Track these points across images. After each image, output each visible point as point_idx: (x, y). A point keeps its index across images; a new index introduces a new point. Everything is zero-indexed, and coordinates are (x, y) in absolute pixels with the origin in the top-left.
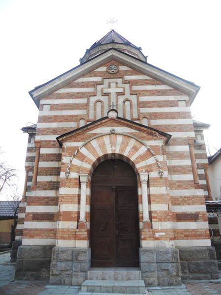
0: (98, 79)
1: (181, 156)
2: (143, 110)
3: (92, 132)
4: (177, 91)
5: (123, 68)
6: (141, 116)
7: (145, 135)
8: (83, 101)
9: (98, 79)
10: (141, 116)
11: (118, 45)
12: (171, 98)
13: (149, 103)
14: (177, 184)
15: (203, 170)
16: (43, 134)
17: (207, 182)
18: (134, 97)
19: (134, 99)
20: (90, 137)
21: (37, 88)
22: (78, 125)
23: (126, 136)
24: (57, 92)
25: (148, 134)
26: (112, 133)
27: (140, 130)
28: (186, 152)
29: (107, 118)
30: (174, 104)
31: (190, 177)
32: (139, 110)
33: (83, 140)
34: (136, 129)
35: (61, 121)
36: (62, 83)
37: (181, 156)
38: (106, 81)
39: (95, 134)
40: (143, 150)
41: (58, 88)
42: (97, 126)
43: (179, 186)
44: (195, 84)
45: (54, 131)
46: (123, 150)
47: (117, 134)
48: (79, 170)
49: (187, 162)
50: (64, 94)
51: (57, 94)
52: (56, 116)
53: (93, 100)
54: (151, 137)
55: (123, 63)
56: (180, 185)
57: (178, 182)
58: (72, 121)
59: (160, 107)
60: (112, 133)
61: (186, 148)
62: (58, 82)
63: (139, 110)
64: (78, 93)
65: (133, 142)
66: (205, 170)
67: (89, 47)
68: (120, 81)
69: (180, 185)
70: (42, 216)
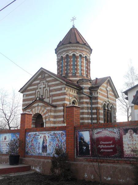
1: (60, 111)
3: (33, 106)
7: (46, 105)
8: (34, 92)
9: (38, 82)
11: (66, 45)
12: (60, 87)
14: (58, 122)
15: (96, 110)
17: (97, 116)
18: (49, 88)
19: (48, 89)
21: (21, 89)
24: (28, 89)
25: (47, 105)
26: (38, 106)
28: (61, 110)
29: (36, 100)
30: (61, 89)
31: (62, 119)
33: (31, 109)
34: (44, 103)
35: (29, 101)
36: (28, 85)
37: (60, 111)
39: (34, 106)
40: (45, 111)
41: (27, 87)
42: (34, 103)
43: (58, 123)
46: (40, 112)
48: (45, 114)
49: (62, 114)
53: (37, 91)
54: (47, 106)
56: (59, 122)
57: (58, 121)
59: (56, 91)
60: (38, 106)
61: (62, 108)
62: (26, 86)
64: (33, 89)
65: (43, 109)
66: (97, 110)
67: (56, 47)
68: (45, 81)
69: (59, 122)
70: (135, 123)
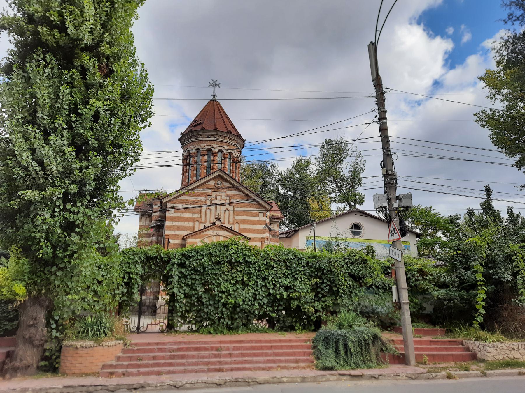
0: (209, 191)
2: (237, 217)
3: (205, 233)
4: (259, 206)
5: (226, 184)
6: (235, 222)
9: (209, 191)
10: (235, 222)
13: (242, 213)
16: (170, 230)
20: (204, 236)
22: (404, 289)
23: (225, 237)
27: (233, 234)
32: (234, 217)
33: (199, 238)
38: (214, 194)
39: (207, 235)
44: (386, 103)
45: (184, 228)
47: (220, 235)
50: (184, 200)
51: (179, 200)
52: (179, 217)
55: (226, 181)
58: (190, 221)
63: (234, 217)
68: (223, 194)
